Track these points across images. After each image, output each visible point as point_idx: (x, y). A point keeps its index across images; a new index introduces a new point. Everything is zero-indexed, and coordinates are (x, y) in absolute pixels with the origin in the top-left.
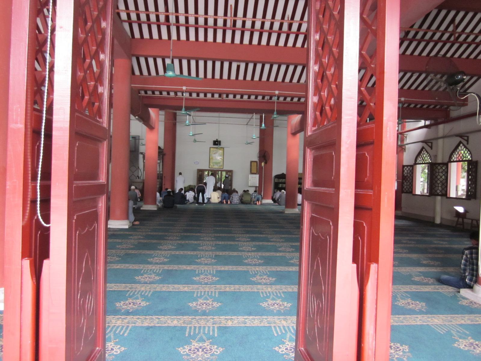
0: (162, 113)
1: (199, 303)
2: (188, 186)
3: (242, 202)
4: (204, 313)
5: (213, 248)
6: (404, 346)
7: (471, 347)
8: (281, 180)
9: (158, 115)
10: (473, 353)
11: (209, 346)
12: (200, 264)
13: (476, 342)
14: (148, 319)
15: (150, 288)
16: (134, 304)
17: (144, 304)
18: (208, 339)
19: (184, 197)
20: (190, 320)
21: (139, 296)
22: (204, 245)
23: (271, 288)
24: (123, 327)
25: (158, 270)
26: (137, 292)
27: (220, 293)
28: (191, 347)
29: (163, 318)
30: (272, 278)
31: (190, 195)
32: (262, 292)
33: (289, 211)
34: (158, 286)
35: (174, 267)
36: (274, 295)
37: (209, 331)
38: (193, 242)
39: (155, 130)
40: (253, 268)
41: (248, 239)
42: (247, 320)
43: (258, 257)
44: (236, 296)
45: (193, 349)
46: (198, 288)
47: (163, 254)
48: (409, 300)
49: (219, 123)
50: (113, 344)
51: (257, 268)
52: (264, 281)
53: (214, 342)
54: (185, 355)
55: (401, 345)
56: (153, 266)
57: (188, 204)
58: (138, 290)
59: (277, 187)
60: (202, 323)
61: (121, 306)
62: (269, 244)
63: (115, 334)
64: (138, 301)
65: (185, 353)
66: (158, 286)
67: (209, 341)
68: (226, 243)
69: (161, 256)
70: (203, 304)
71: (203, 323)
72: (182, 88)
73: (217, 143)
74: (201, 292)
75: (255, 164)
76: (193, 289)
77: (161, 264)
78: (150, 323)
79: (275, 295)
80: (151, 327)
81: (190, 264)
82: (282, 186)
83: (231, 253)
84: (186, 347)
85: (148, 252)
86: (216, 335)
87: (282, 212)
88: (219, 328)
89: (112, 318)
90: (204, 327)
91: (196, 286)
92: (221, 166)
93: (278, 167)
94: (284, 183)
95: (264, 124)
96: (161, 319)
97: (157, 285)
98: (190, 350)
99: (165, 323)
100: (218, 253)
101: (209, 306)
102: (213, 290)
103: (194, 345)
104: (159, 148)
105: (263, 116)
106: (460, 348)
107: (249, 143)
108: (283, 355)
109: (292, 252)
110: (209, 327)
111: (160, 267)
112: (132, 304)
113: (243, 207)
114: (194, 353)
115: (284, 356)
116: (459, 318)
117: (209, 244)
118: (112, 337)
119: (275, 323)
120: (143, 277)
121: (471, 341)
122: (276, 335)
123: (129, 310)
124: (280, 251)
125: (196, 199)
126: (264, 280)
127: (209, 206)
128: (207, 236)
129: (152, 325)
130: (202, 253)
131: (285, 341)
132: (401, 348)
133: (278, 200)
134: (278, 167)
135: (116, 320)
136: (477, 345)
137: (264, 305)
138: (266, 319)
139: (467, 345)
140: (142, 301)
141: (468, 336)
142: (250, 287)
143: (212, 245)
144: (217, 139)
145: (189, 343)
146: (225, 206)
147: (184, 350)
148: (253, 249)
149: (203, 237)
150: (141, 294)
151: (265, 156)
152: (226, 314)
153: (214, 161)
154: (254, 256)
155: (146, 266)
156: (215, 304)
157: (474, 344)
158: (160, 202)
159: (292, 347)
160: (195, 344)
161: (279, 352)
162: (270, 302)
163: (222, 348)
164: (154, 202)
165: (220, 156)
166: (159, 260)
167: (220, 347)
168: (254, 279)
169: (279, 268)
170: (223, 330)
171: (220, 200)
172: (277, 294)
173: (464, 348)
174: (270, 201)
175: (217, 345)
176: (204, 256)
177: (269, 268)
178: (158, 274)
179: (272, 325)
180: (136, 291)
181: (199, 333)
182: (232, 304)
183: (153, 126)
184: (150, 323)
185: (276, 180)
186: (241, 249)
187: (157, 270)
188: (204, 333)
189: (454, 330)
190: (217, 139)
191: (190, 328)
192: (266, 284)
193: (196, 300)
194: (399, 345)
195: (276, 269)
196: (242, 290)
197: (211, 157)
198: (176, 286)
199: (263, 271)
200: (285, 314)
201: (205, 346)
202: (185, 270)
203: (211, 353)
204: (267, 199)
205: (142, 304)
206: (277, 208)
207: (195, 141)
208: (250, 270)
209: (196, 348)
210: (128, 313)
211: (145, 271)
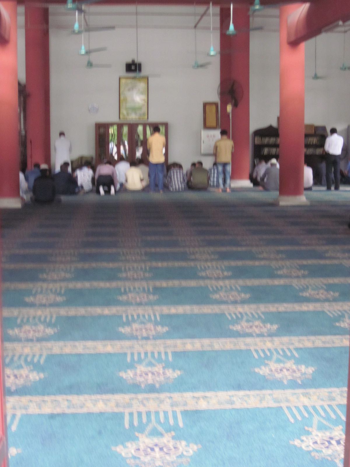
0: (21, 9)
1: (138, 372)
2: (79, 159)
3: (190, 186)
4: (152, 389)
5: (147, 275)
8: (266, 140)
9: (15, 14)
12: (128, 303)
19: (73, 181)
21: (23, 363)
23: (272, 341)
27: (175, 354)
29: (76, 399)
31: (84, 177)
32: (257, 351)
33: (288, 201)
36: (278, 353)
37: (166, 417)
38: (105, 265)
39: (11, 45)
42: (234, 399)
43: (296, 355)
46: (132, 347)
49: (137, 27)
51: (240, 309)
52: (257, 331)
57: (81, 193)
58: (17, 355)
59: (260, 155)
60: (152, 406)
62: (257, 263)
63: (26, 360)
64: (24, 372)
68: (170, 264)
73: (133, 67)
75: (214, 108)
77: (51, 305)
80: (58, 415)
81: (108, 303)
82: (269, 152)
83: (185, 283)
85: (22, 286)
86: (181, 424)
87: (274, 204)
88: (186, 413)
90: (157, 413)
91: (127, 343)
92: (144, 114)
93: (262, 113)
94: (276, 146)
95: (233, 22)
99: (82, 407)
100: (158, 284)
102: (162, 350)
103: (144, 442)
104: (19, 84)
105: (230, 9)
107: (202, 66)
108: (309, 452)
109: (304, 276)
110: (166, 413)
113: (193, 196)
119: (288, 401)
122: (292, 420)
124: (280, 277)
125: (97, 182)
127: (123, 197)
129: (58, 410)
130: (128, 284)
133: (262, 179)
134: (262, 113)
137: (263, 371)
145: (135, 439)
146: (159, 196)
151: (233, 89)
152: (194, 388)
153: (129, 105)
158: (26, 192)
159: (325, 438)
160: (145, 441)
162: (273, 366)
163: (196, 444)
164: (15, 191)
165: (142, 93)
168: (237, 328)
169: (283, 307)
170: (193, 415)
171: (145, 183)
174: (247, 183)
175: (186, 440)
176: (143, 356)
177: (263, 308)
178: (49, 325)
179: (284, 405)
181: (149, 420)
182: (201, 372)
183: (6, 37)
185: (258, 141)
187: (46, 318)
188: (159, 422)
191: (131, 414)
192: (261, 335)
193: (131, 366)
196: (217, 347)
197: (122, 98)
198: (90, 344)
200: (304, 385)
202: (100, 316)
204: (240, 178)
206: (260, 195)
207: (90, 64)
208: (226, 313)
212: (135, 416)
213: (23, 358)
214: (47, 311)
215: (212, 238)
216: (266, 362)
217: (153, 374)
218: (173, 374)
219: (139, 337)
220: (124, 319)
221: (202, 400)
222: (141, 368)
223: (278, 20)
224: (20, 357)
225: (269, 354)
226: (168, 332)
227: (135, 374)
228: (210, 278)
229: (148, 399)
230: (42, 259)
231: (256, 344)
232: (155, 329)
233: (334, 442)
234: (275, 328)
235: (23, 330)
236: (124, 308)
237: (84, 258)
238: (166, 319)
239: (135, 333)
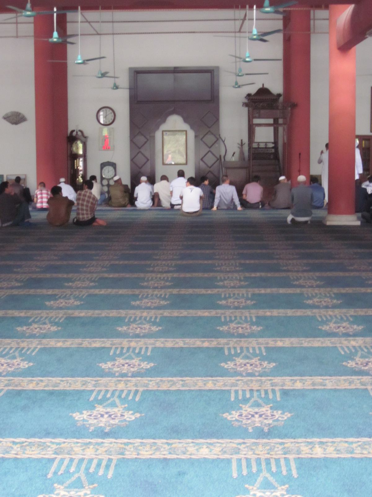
5: (249, 302)
14: (148, 446)
15: (136, 385)
16: (8, 365)
22: (230, 297)
24: (130, 391)
25: (143, 350)
26: (75, 463)
27: (268, 349)
29: (177, 444)
34: (151, 381)
35: (177, 343)
36: (362, 350)
40: (345, 342)
56: (131, 341)
58: (111, 389)
66: (151, 381)
70: (102, 416)
71: (263, 452)
74: (244, 391)
78: (154, 454)
89: (74, 443)
91: (231, 380)
96: (174, 446)
97: (126, 441)
100: (261, 312)
101: (266, 419)
102: (269, 388)
111: (145, 344)
117: (238, 294)
120: (95, 413)
128: (225, 264)
129: (158, 455)
135: (81, 446)
142: (345, 380)
149: (221, 280)
150: (119, 396)
155: (117, 341)
167: (286, 412)
178: (154, 323)
180: (107, 391)
184: (154, 454)
187: (141, 349)
201: (263, 411)
211: (118, 352)
212: (244, 463)
214: (165, 275)
215: (308, 251)
216: (327, 323)
218: (282, 416)
219: (229, 287)
220: (223, 320)
221: (317, 446)
223: (327, 22)
225: (353, 351)
226: (254, 304)
228: (318, 307)
229: (257, 444)
230: (135, 284)
232: (250, 328)
234: (361, 329)
236: (223, 311)
237: (178, 283)
238: (271, 353)
239: (226, 285)
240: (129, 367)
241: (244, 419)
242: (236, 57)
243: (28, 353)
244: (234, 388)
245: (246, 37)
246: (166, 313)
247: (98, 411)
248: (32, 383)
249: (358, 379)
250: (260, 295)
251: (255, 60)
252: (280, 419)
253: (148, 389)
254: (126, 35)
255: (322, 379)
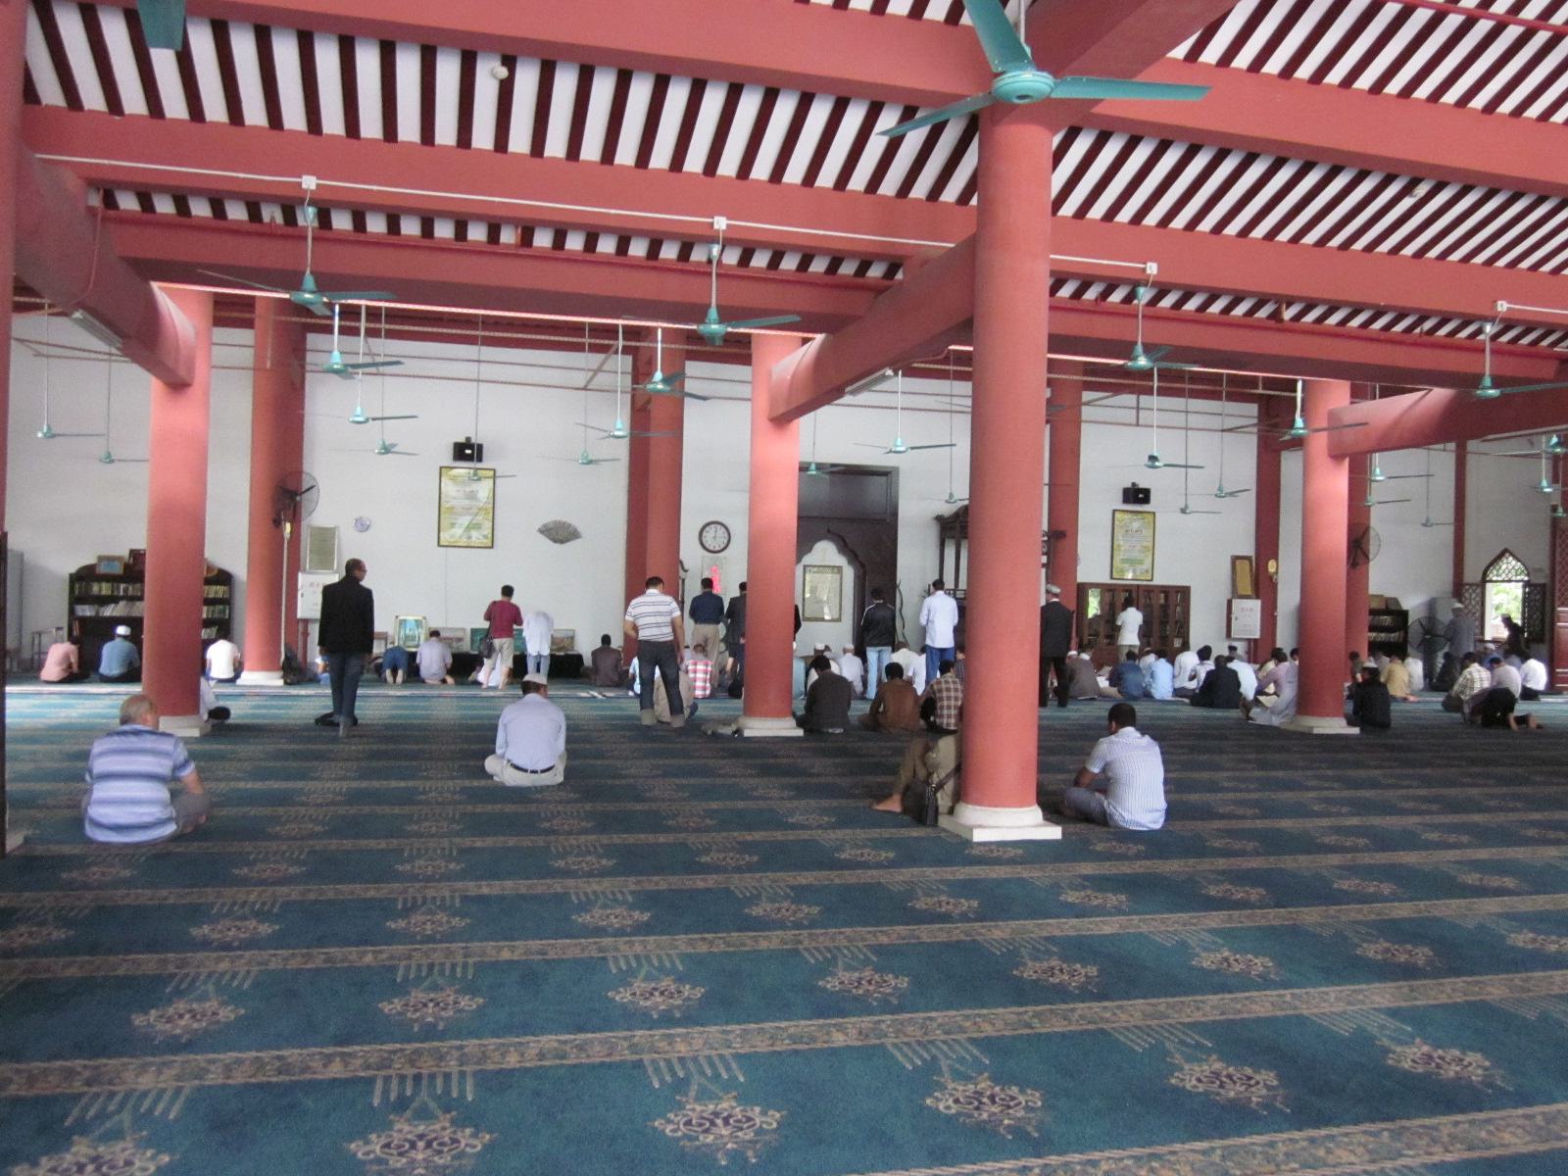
6: (1029, 1091)
7: (1213, 1083)
10: (1218, 1098)
11: (448, 1131)
13: (1227, 1068)
16: (194, 1017)
17: (227, 1014)
18: (447, 1111)
20: (386, 1055)
21: (211, 987)
27: (484, 1079)
28: (391, 1136)
30: (693, 988)
41: (584, 824)
43: (630, 899)
44: (530, 976)
45: (396, 1142)
47: (284, 852)
48: (1055, 962)
50: (130, 1145)
51: (596, 886)
53: (468, 1117)
54: (371, 1162)
55: (1022, 1091)
61: (149, 1025)
62: (662, 839)
63: (217, 984)
64: (211, 1005)
65: (372, 1156)
67: (448, 1116)
69: (247, 910)
70: (425, 1005)
72: (300, 184)
73: (467, 452)
76: (392, 958)
79: (709, 1072)
84: (373, 1137)
90: (432, 1077)
91: (399, 949)
98: (387, 1145)
106: (1184, 1087)
107: (590, 462)
110: (447, 1076)
112: (187, 1016)
114: (401, 1154)
115: (681, 1143)
116: (1189, 1006)
118: (127, 1124)
121: (1217, 1066)
123: (180, 1036)
124: (707, 869)
126: (615, 921)
130: (413, 890)
131: (684, 1100)
132: (1022, 1099)
136: (1230, 1077)
137: (623, 996)
138: (625, 1039)
139: (1204, 1080)
140: (224, 1004)
141: (1209, 1052)
143: (447, 852)
144: (468, 439)
145: (388, 1126)
147: (368, 1148)
148: (584, 824)
154: (613, 893)
156: (465, 1002)
157: (1224, 1073)
159: (705, 1115)
161: (665, 1135)
166: (273, 870)
170: (497, 1082)
172: (712, 1065)
173: (1195, 1087)
176: (423, 852)
179: (646, 1057)
180: (112, 1095)
183: (182, 373)
186: (561, 863)
189: (1173, 1041)
190: (468, 439)
191: (387, 1079)
194: (1015, 1090)
195: (657, 884)
199: (613, 893)
203: (454, 1152)
205: (221, 1014)
209: (406, 1140)
210: (175, 1046)
213: (436, 969)
217: (433, 923)
222: (417, 995)
224: (210, 975)
227: (413, 867)
231: (617, 949)
233: (719, 1122)
235: (256, 868)
240: (437, 1009)
241: (392, 1155)
242: (586, 426)
243: (235, 983)
244: (383, 1073)
245: (1538, 456)
246: (294, 893)
247: (75, 1154)
248: (128, 1070)
249: (625, 1039)
250: (472, 850)
251: (912, 448)
252: (468, 1150)
253: (203, 1083)
254: (423, 380)
255: (559, 1041)
